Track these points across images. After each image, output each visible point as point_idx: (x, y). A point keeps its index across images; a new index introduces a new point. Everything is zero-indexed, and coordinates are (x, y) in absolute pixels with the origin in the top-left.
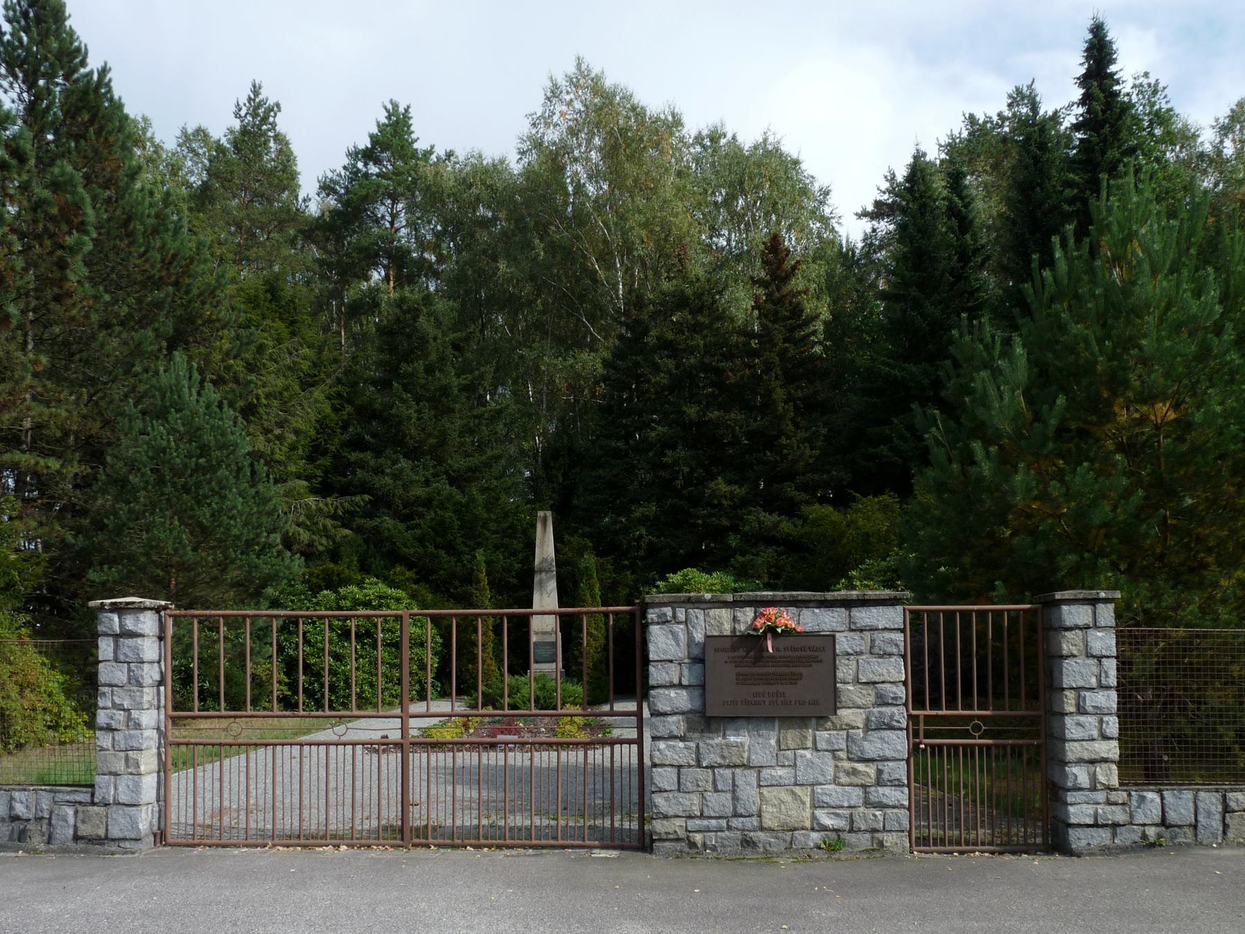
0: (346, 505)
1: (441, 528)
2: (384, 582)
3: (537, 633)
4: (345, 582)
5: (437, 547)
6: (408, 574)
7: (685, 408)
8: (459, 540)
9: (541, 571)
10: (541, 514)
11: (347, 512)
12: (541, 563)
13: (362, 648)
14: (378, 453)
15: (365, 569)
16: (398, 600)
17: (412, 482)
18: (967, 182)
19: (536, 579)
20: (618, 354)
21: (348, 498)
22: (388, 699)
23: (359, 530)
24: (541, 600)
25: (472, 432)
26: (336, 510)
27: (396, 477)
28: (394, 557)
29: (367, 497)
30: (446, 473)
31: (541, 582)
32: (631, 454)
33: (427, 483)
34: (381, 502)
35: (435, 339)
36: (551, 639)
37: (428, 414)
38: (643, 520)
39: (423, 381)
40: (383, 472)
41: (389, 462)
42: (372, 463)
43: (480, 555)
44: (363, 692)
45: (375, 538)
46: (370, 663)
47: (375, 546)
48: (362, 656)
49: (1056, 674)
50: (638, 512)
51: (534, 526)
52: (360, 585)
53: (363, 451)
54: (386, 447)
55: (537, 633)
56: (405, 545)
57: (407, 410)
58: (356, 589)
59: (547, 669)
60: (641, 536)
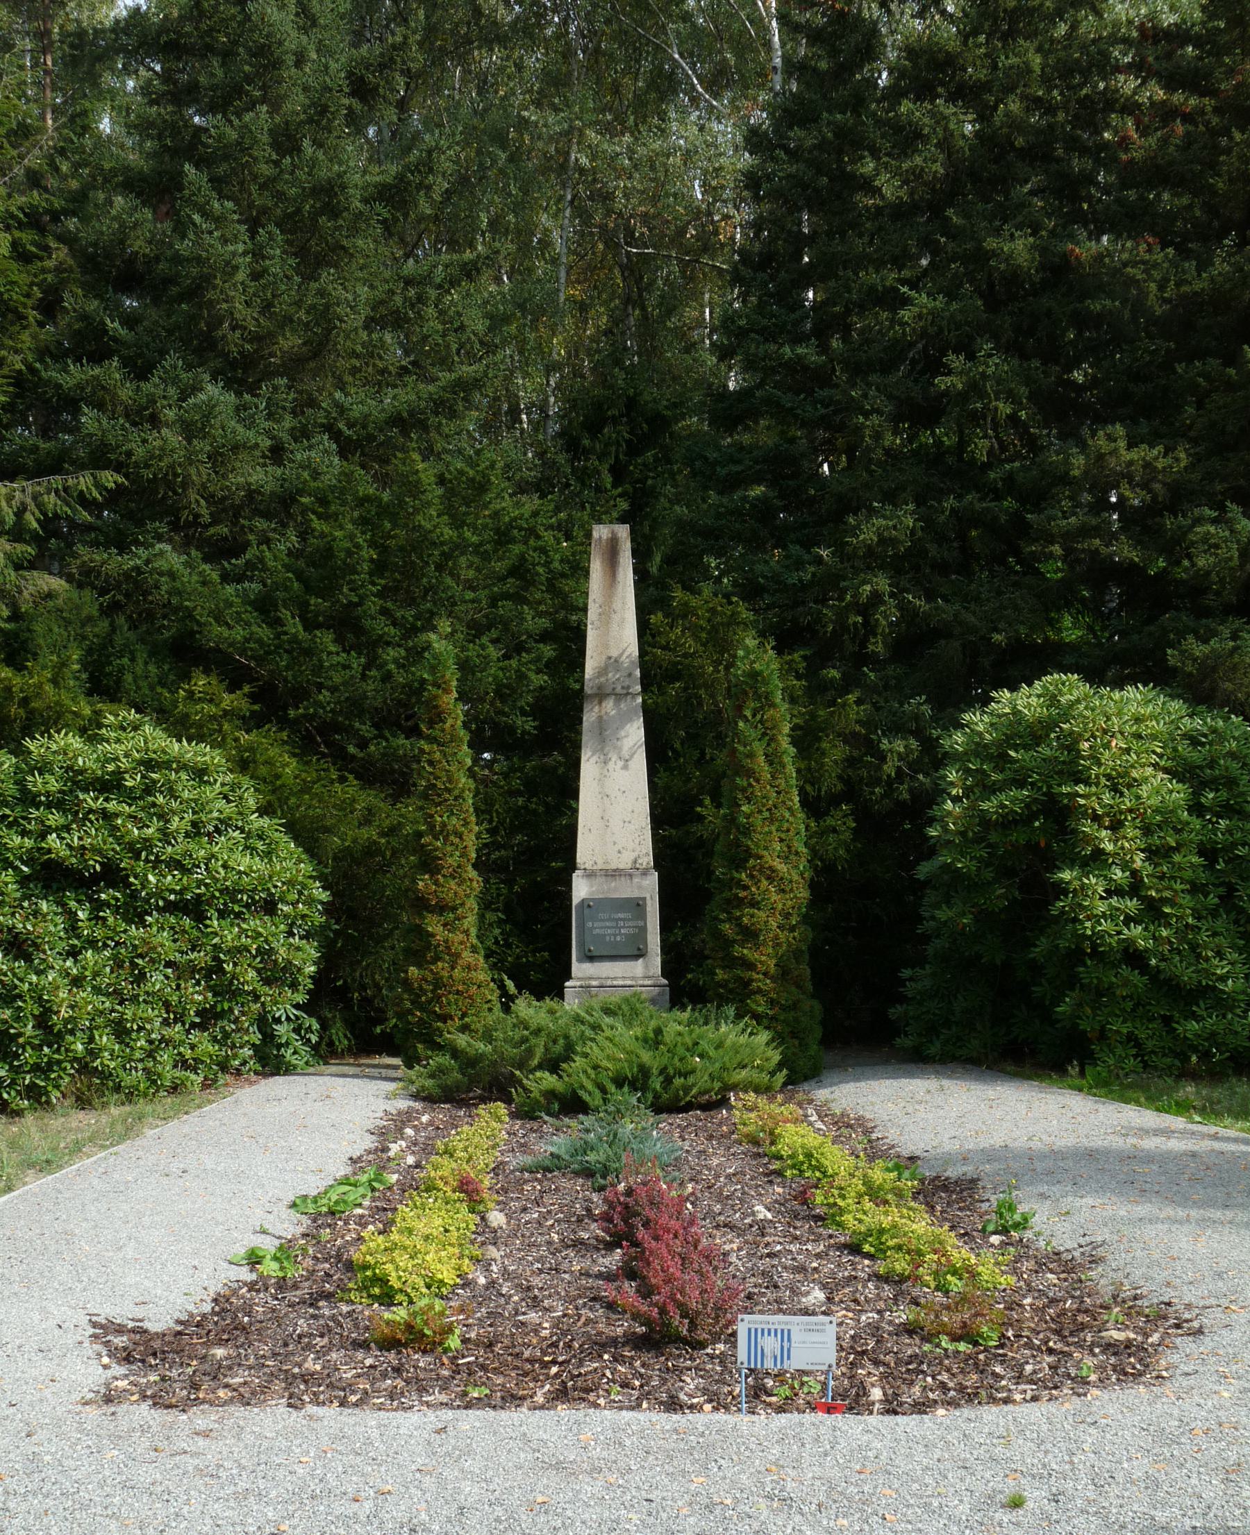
0: (51, 500)
1: (320, 570)
2: (158, 723)
3: (590, 875)
4: (44, 721)
5: (309, 625)
6: (228, 700)
7: (991, 243)
8: (373, 605)
9: (601, 696)
10: (601, 532)
11: (50, 523)
12: (602, 671)
13: (95, 918)
14: (140, 370)
15: (103, 686)
16: (200, 774)
17: (235, 448)
18: (313, 969)
19: (589, 717)
20: (792, 114)
21: (57, 481)
22: (169, 1073)
23: (85, 579)
24: (601, 780)
25: (397, 321)
26: (20, 513)
27: (190, 431)
28: (187, 653)
29: (110, 479)
30: (330, 428)
31: (601, 724)
32: (840, 375)
33: (277, 453)
34: (145, 502)
35: (300, 61)
36: (625, 890)
37: (278, 261)
38: (873, 558)
39: (265, 170)
40: (155, 421)
41: (172, 391)
42: (126, 392)
43: (440, 641)
44: (93, 1053)
45: (128, 599)
46: (118, 964)
47: (134, 626)
48: (92, 943)
49: (938, 1067)
50: (868, 532)
51: (583, 572)
52: (90, 731)
53: (98, 358)
54: (163, 353)
55: (590, 875)
56: (219, 619)
57: (218, 237)
58: (76, 742)
59: (615, 978)
60: (876, 597)
